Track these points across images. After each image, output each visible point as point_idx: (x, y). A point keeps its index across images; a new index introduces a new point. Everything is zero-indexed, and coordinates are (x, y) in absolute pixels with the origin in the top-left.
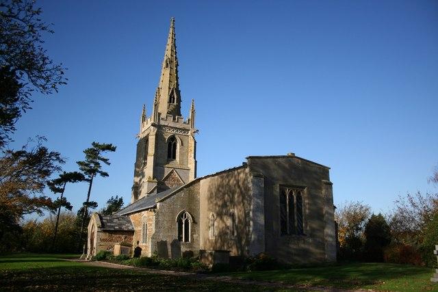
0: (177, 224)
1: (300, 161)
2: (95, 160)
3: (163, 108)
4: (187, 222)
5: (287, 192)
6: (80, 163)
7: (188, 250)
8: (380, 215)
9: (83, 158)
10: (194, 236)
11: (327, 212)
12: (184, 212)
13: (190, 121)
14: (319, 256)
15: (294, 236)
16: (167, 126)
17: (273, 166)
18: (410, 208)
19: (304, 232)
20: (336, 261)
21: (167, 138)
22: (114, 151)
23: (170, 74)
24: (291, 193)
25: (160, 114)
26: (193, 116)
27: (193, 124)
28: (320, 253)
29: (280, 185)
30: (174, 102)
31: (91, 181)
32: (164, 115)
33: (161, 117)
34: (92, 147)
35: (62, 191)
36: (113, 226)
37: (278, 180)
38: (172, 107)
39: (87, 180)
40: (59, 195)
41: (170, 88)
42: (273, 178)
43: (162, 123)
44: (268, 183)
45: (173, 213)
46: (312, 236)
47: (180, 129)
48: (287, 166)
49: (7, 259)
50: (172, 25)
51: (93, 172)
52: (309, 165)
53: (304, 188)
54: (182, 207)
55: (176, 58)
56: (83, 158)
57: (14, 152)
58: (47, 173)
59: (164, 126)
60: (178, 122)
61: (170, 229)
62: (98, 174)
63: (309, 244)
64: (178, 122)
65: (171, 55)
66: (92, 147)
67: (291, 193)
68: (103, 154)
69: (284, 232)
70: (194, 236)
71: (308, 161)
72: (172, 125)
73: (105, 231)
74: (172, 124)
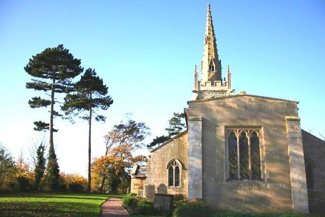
0: (167, 171)
1: (253, 99)
2: (177, 126)
4: (177, 168)
7: (178, 193)
8: (154, 140)
9: (168, 126)
10: (184, 181)
11: (292, 154)
12: (174, 160)
13: (227, 84)
14: (282, 205)
15: (245, 181)
16: (206, 91)
19: (262, 177)
20: (308, 212)
21: (237, 107)
22: (30, 102)
23: (209, 49)
24: (243, 134)
25: (199, 82)
28: (284, 202)
29: (226, 127)
30: (213, 70)
32: (203, 83)
33: (201, 84)
34: (174, 116)
37: (222, 121)
38: (212, 74)
41: (209, 60)
42: (215, 120)
43: (202, 89)
45: (163, 160)
46: (270, 181)
47: (218, 91)
48: (235, 106)
49: (72, 196)
50: (208, 10)
53: (260, 127)
54: (172, 155)
55: (214, 34)
59: (204, 91)
60: (216, 86)
61: (161, 175)
63: (267, 190)
64: (216, 86)
65: (209, 34)
67: (243, 134)
69: (232, 177)
73: (137, 178)
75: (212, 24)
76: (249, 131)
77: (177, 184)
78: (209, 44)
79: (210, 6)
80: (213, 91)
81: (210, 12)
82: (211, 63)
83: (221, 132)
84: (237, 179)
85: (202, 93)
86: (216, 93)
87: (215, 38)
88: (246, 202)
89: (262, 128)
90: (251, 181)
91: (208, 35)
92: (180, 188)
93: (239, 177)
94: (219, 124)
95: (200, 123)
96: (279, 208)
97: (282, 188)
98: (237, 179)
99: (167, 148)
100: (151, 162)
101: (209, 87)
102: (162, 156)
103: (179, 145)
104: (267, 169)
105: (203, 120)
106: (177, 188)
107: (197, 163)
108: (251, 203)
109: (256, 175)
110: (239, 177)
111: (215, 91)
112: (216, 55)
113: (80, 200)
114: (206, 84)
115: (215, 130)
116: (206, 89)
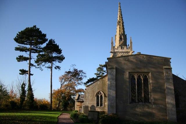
0: (96, 97)
2: (102, 72)
3: (117, 44)
4: (101, 96)
6: (95, 74)
7: (102, 111)
9: (96, 72)
11: (167, 88)
12: (99, 91)
13: (130, 48)
15: (140, 103)
16: (118, 52)
17: (122, 60)
18: (3, 82)
20: (176, 121)
25: (114, 47)
26: (131, 45)
27: (131, 50)
29: (129, 73)
30: (122, 40)
32: (116, 47)
34: (100, 66)
38: (121, 42)
41: (119, 34)
43: (116, 51)
44: (119, 72)
45: (93, 92)
46: (154, 103)
48: (134, 60)
50: (119, 6)
52: (152, 58)
54: (98, 89)
55: (122, 20)
57: (67, 72)
58: (81, 79)
59: (117, 52)
60: (123, 49)
61: (92, 100)
63: (152, 108)
64: (123, 49)
66: (100, 66)
67: (139, 76)
69: (133, 101)
70: (105, 103)
71: (150, 55)
72: (121, 51)
74: (121, 51)
75: (121, 14)
76: (142, 75)
78: (120, 25)
79: (120, 4)
80: (122, 52)
81: (120, 7)
82: (121, 36)
83: (127, 75)
84: (136, 102)
87: (123, 22)
92: (103, 108)
93: (137, 101)
95: (115, 70)
98: (136, 102)
99: (96, 85)
100: (87, 93)
101: (120, 50)
104: (153, 96)
105: (116, 69)
110: (137, 101)
111: (123, 52)
112: (124, 31)
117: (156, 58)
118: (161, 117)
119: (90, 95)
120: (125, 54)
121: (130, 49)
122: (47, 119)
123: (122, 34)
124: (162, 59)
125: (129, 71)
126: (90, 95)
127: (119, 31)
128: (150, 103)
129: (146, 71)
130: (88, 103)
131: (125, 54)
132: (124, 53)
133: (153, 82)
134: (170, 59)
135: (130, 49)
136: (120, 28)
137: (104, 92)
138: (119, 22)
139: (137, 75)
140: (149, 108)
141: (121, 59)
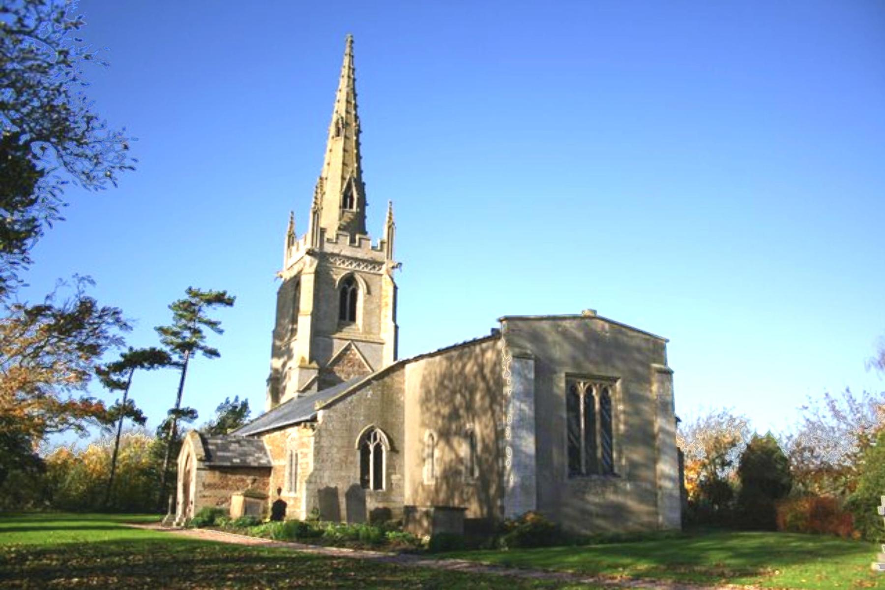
0: (358, 454)
1: (607, 326)
2: (191, 324)
3: (331, 218)
5: (582, 388)
9: (168, 320)
11: (662, 430)
12: (372, 429)
13: (385, 246)
15: (594, 477)
16: (338, 255)
24: (589, 391)
25: (323, 231)
30: (351, 207)
31: (184, 367)
32: (331, 234)
33: (327, 236)
35: (125, 386)
36: (229, 459)
38: (348, 216)
39: (176, 364)
40: (119, 394)
41: (343, 178)
42: (552, 360)
43: (328, 248)
45: (350, 430)
47: (364, 261)
48: (580, 335)
50: (348, 50)
51: (188, 347)
53: (615, 380)
54: (368, 418)
55: (356, 117)
56: (168, 320)
57: (29, 307)
58: (94, 350)
59: (333, 255)
60: (359, 246)
61: (344, 463)
62: (199, 353)
63: (626, 493)
64: (359, 246)
65: (347, 112)
67: (589, 391)
68: (211, 312)
69: (574, 470)
74: (348, 251)
75: (354, 89)
76: (598, 386)
77: (295, 490)
78: (346, 137)
79: (352, 42)
80: (352, 258)
81: (353, 57)
82: (349, 187)
83: (561, 385)
84: (583, 475)
85: (328, 259)
86: (366, 266)
87: (359, 126)
88: (598, 516)
89: (618, 384)
90: (602, 478)
91: (344, 115)
92: (384, 494)
93: (584, 470)
94: (558, 368)
95: (531, 363)
96: (642, 525)
97: (646, 490)
98: (580, 473)
99: (359, 401)
100: (324, 433)
101: (344, 248)
102: (348, 419)
103: (383, 394)
104: (622, 458)
105: (537, 360)
106: (378, 494)
107: (529, 444)
108: (604, 516)
109: (608, 471)
110: (584, 470)
111: (356, 259)
112: (359, 171)
113: (109, 532)
114: (337, 238)
115: (551, 380)
116: (336, 251)
117: (635, 334)
118: (646, 519)
119: (338, 443)
120: (350, 267)
121: (385, 250)
122: (113, 547)
123: (355, 180)
124: (647, 340)
125: (569, 370)
126: (338, 443)
127: (344, 164)
128: (615, 475)
129: (611, 373)
130: (329, 477)
131: (350, 267)
132: (359, 265)
133: (628, 409)
134: (667, 341)
135: (385, 250)
136: (345, 150)
137: (388, 432)
138: (346, 125)
139: (585, 384)
140: (616, 492)
141: (546, 325)
